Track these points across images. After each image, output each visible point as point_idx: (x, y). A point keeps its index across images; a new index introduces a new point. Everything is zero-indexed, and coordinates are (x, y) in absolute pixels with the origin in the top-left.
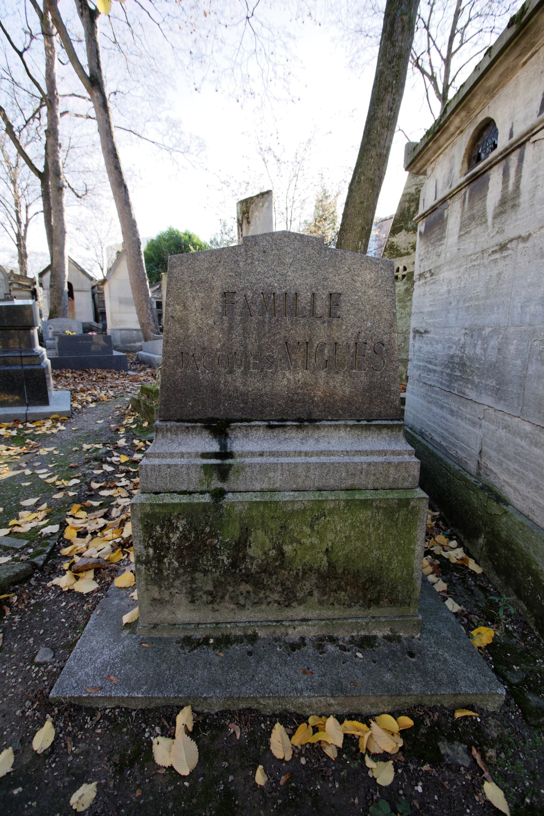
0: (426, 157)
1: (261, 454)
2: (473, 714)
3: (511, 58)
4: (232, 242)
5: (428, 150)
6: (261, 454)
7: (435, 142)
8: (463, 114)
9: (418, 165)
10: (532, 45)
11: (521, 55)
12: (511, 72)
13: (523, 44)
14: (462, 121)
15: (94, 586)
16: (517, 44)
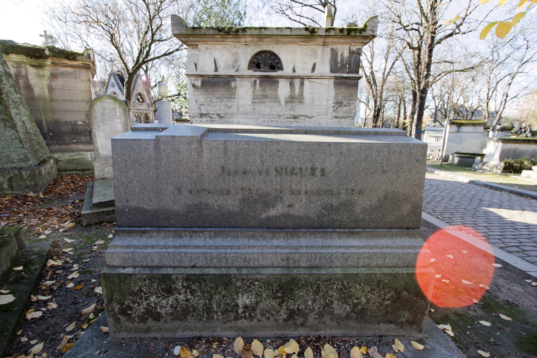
0: (205, 39)
1: (403, 247)
2: (73, 241)
3: (298, 40)
4: (304, 232)
5: (213, 37)
6: (403, 247)
7: (222, 38)
8: (256, 39)
9: (191, 39)
10: (308, 42)
11: (302, 42)
12: (293, 43)
13: (306, 40)
14: (251, 41)
15: (397, 341)
16: (305, 38)
